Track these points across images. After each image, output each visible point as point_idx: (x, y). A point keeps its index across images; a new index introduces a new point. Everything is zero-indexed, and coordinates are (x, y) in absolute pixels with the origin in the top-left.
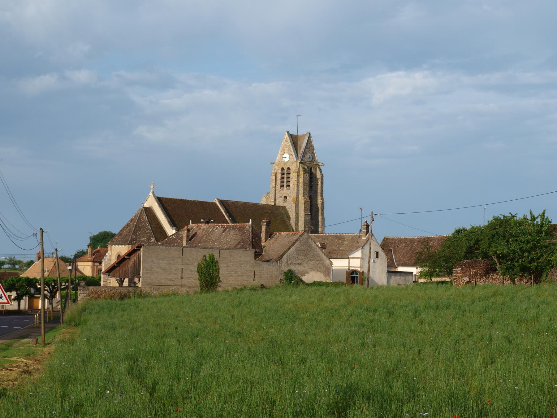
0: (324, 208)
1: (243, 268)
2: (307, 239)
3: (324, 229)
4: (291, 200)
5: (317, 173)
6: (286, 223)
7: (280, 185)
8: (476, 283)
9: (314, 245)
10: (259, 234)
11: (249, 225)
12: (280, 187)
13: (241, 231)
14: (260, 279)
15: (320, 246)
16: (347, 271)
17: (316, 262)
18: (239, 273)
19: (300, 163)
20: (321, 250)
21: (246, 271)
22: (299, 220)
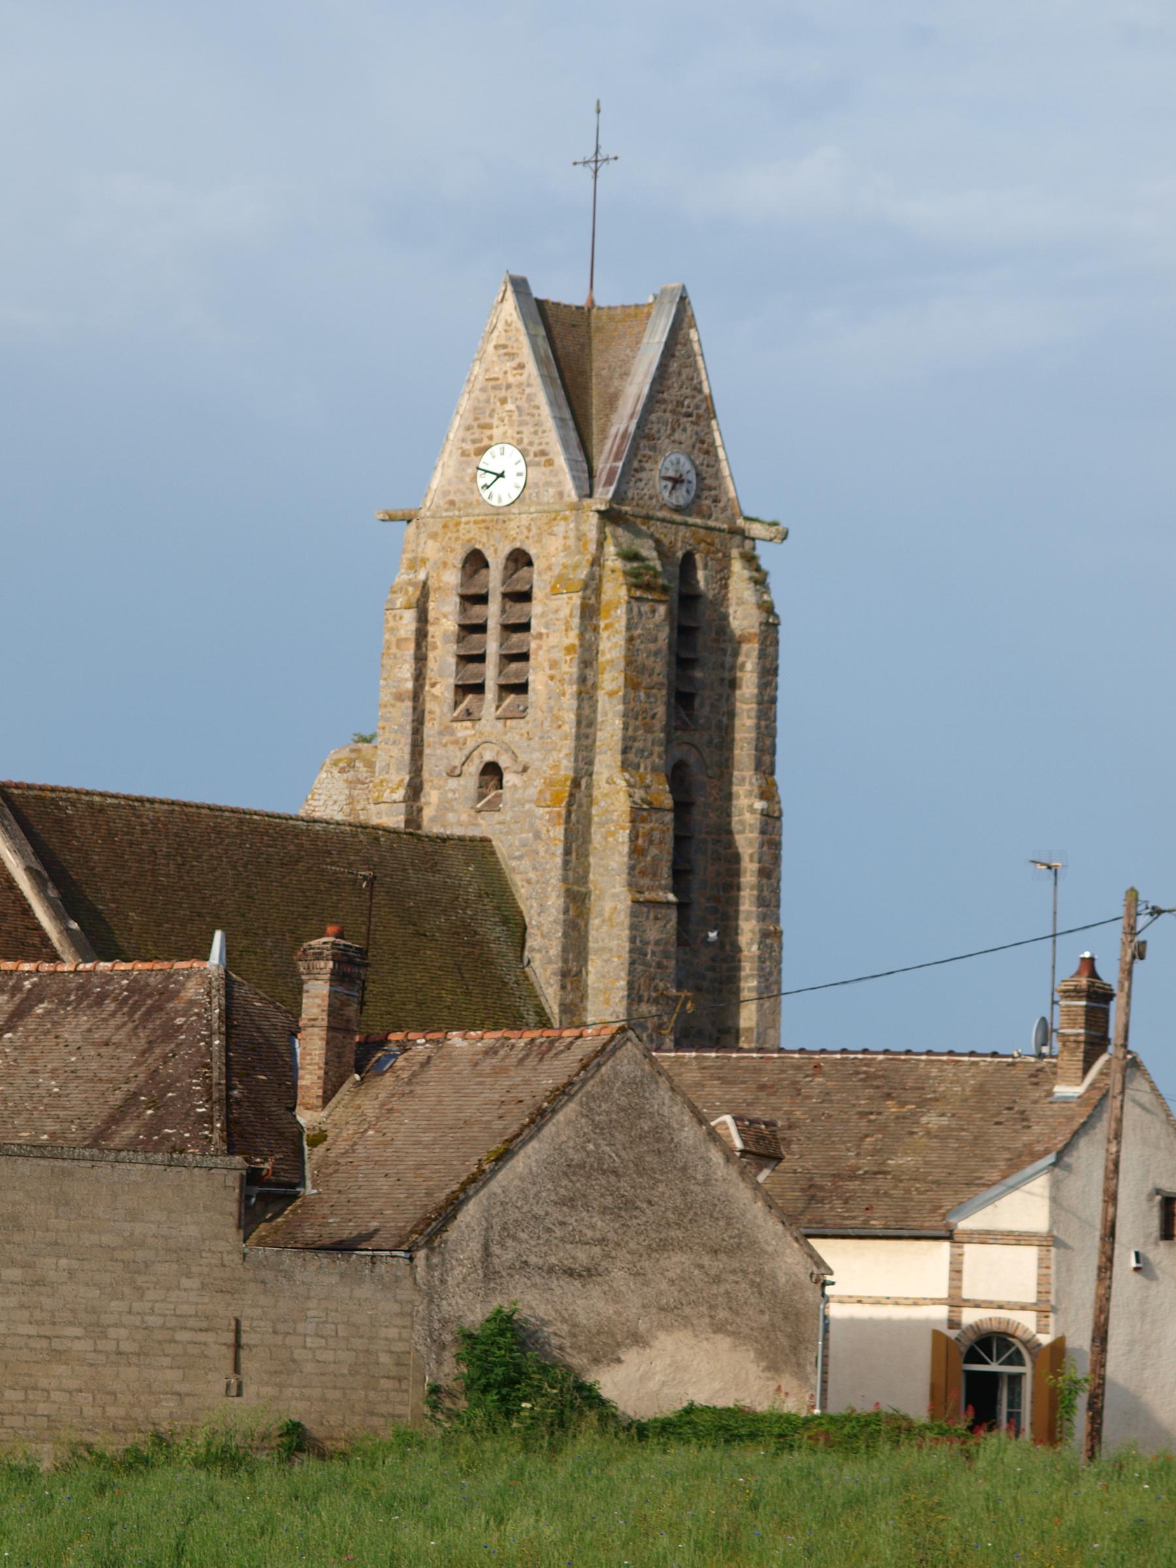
0: (776, 859)
1: (150, 1295)
2: (636, 1085)
3: (776, 1012)
4: (532, 792)
5: (732, 595)
6: (489, 963)
7: (452, 681)
8: (368, 934)
9: (689, 1134)
10: (282, 1047)
11: (203, 975)
12: (449, 695)
13: (149, 1013)
14: (281, 1386)
15: (738, 1144)
16: (937, 1335)
17: (706, 1260)
18: (123, 1332)
19: (609, 516)
20: (742, 1173)
21: (173, 1322)
22: (591, 945)
